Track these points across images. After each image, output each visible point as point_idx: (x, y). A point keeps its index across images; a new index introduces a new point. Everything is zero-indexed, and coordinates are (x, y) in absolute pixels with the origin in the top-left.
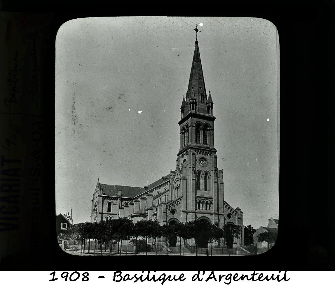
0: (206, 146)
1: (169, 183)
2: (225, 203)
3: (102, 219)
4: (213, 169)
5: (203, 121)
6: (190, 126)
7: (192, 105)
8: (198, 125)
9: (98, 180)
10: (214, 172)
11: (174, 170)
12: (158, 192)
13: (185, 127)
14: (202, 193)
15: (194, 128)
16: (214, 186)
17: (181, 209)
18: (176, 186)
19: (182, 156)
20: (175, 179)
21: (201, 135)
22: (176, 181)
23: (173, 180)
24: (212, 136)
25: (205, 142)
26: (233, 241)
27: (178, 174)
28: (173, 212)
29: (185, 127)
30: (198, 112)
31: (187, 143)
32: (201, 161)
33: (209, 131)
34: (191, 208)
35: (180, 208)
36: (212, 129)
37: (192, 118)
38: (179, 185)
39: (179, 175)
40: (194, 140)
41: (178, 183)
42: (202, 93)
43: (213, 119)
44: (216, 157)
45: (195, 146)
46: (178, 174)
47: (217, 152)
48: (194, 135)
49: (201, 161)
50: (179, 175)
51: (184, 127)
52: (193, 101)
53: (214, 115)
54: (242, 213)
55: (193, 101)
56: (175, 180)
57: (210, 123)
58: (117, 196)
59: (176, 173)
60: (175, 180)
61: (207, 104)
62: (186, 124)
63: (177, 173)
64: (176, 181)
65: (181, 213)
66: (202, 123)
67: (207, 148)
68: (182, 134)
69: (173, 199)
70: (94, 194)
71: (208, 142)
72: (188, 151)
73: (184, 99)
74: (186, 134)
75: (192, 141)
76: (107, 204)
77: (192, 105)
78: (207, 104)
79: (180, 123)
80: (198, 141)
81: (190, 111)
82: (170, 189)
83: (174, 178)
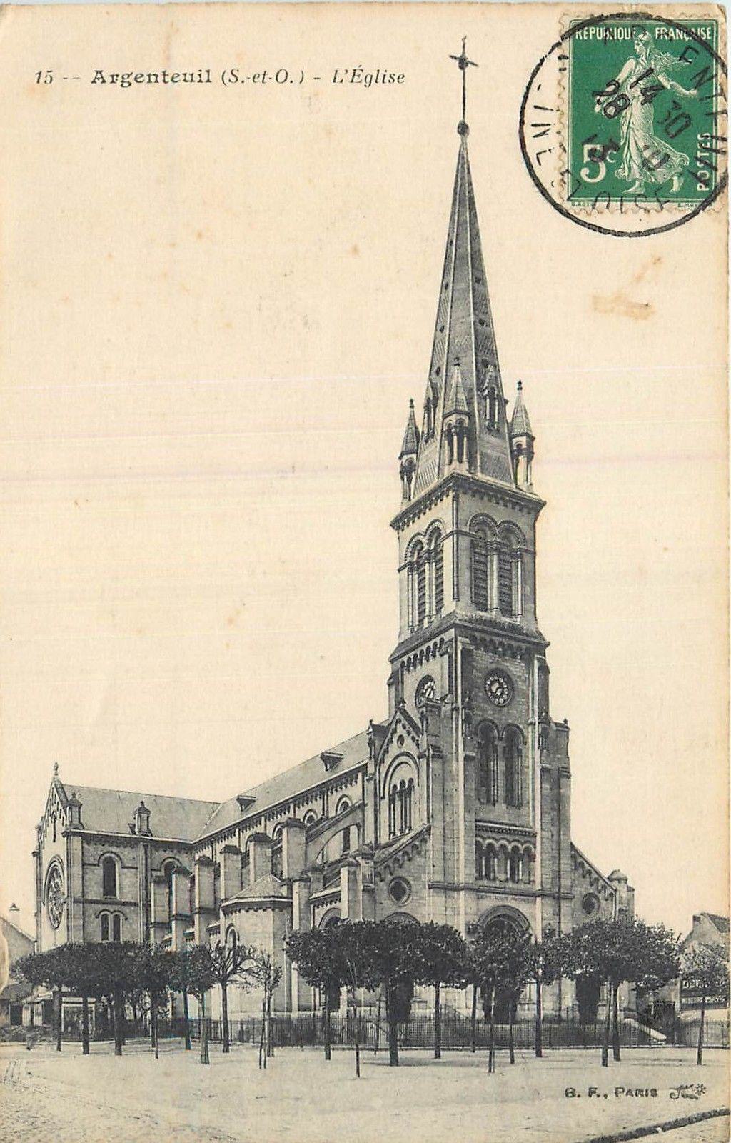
0: (508, 620)
1: (360, 775)
2: (576, 855)
3: (316, 859)
4: (536, 718)
5: (500, 514)
6: (452, 533)
7: (455, 438)
8: (481, 522)
9: (54, 772)
10: (538, 729)
11: (382, 717)
12: (344, 799)
13: (425, 541)
14: (500, 813)
15: (465, 542)
16: (538, 785)
17: (425, 878)
18: (395, 786)
19: (415, 663)
20: (388, 761)
21: (492, 575)
22: (396, 763)
23: (382, 761)
24: (530, 582)
25: (506, 609)
26: (410, 994)
27: (405, 735)
28: (398, 891)
29: (425, 541)
30: (479, 474)
31: (417, 618)
32: (490, 686)
33: (521, 556)
34: (463, 872)
35: (425, 868)
36: (531, 548)
37: (456, 499)
38: (411, 781)
39: (408, 740)
40: (466, 591)
41: (405, 773)
42: (493, 389)
43: (536, 507)
44: (544, 670)
45: (470, 620)
46: (405, 735)
47: (547, 650)
48: (466, 576)
49: (492, 683)
50: (408, 740)
51: (420, 538)
52: (461, 422)
53: (540, 492)
54: (631, 890)
55: (461, 422)
56: (393, 762)
57: (522, 521)
58: (134, 833)
59: (395, 731)
60: (393, 762)
61: (511, 438)
62: (415, 535)
63: (400, 731)
64: (396, 763)
65: (426, 892)
66: (493, 520)
67: (513, 628)
68: (411, 571)
69: (384, 839)
70: (39, 828)
71: (517, 607)
72: (442, 640)
73: (412, 418)
74: (429, 571)
75: (457, 597)
76: (101, 865)
77: (455, 438)
78: (511, 438)
79: (399, 523)
80: (480, 601)
81: (447, 468)
82: (370, 801)
83: (387, 751)
